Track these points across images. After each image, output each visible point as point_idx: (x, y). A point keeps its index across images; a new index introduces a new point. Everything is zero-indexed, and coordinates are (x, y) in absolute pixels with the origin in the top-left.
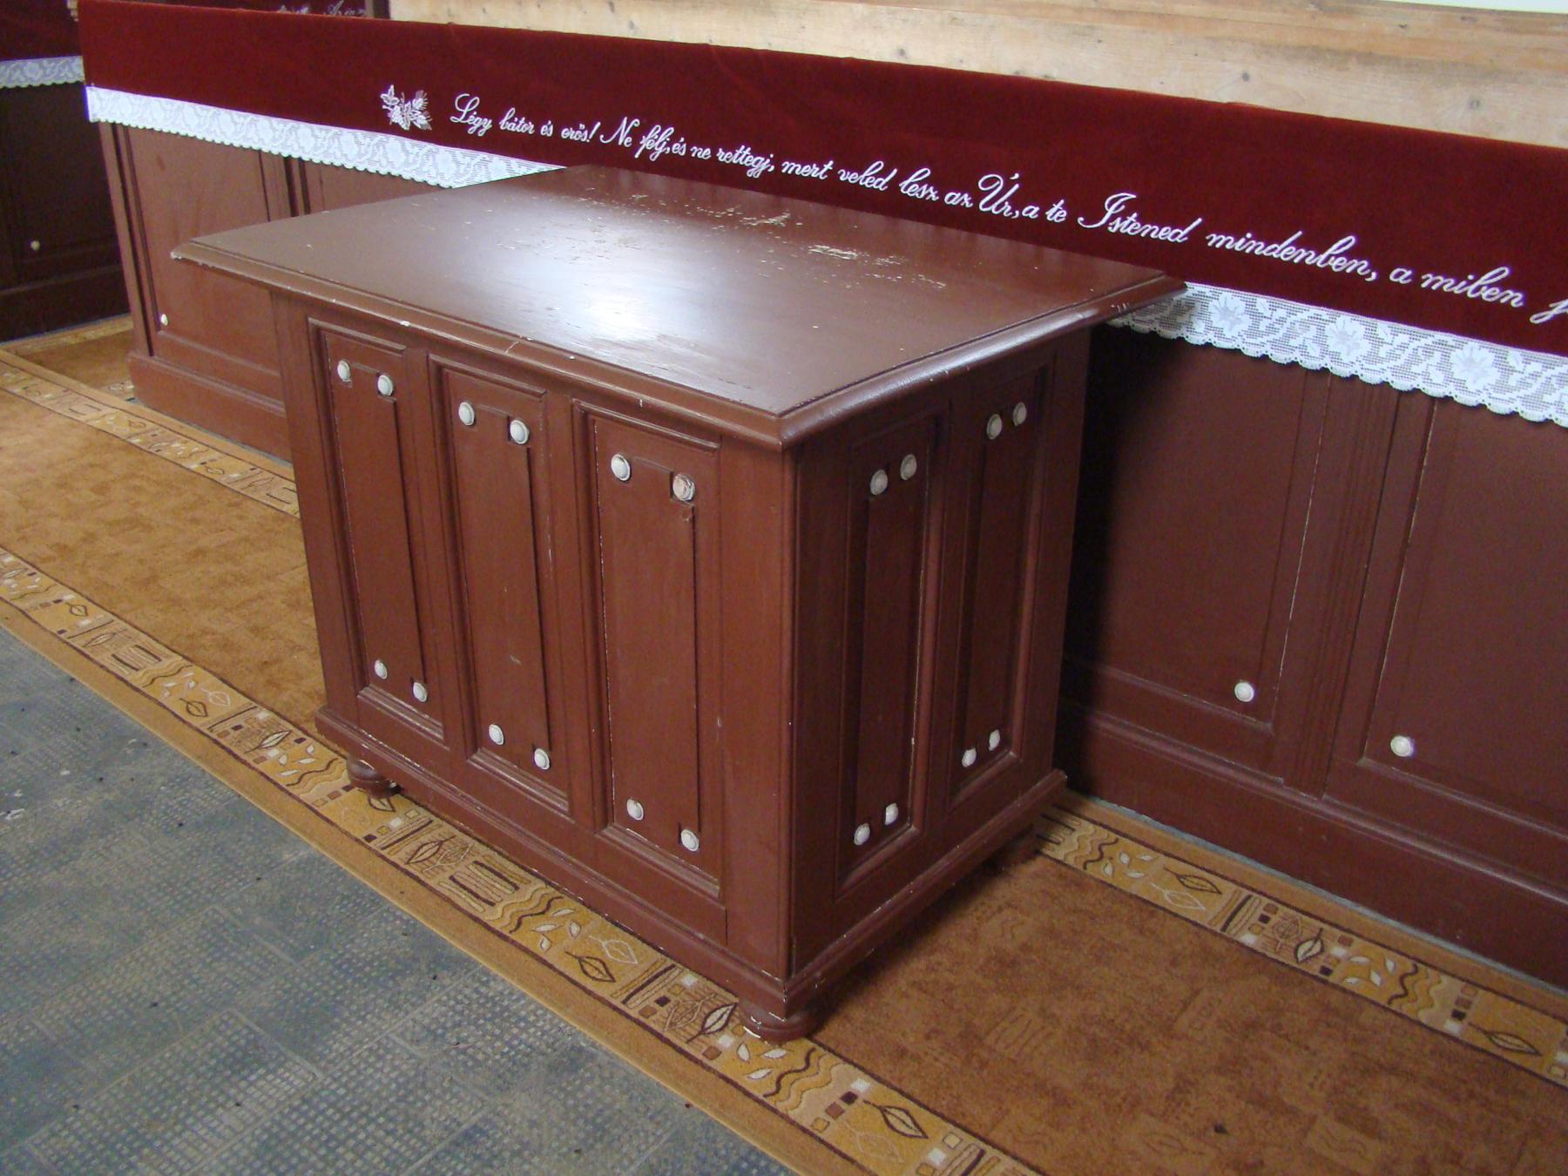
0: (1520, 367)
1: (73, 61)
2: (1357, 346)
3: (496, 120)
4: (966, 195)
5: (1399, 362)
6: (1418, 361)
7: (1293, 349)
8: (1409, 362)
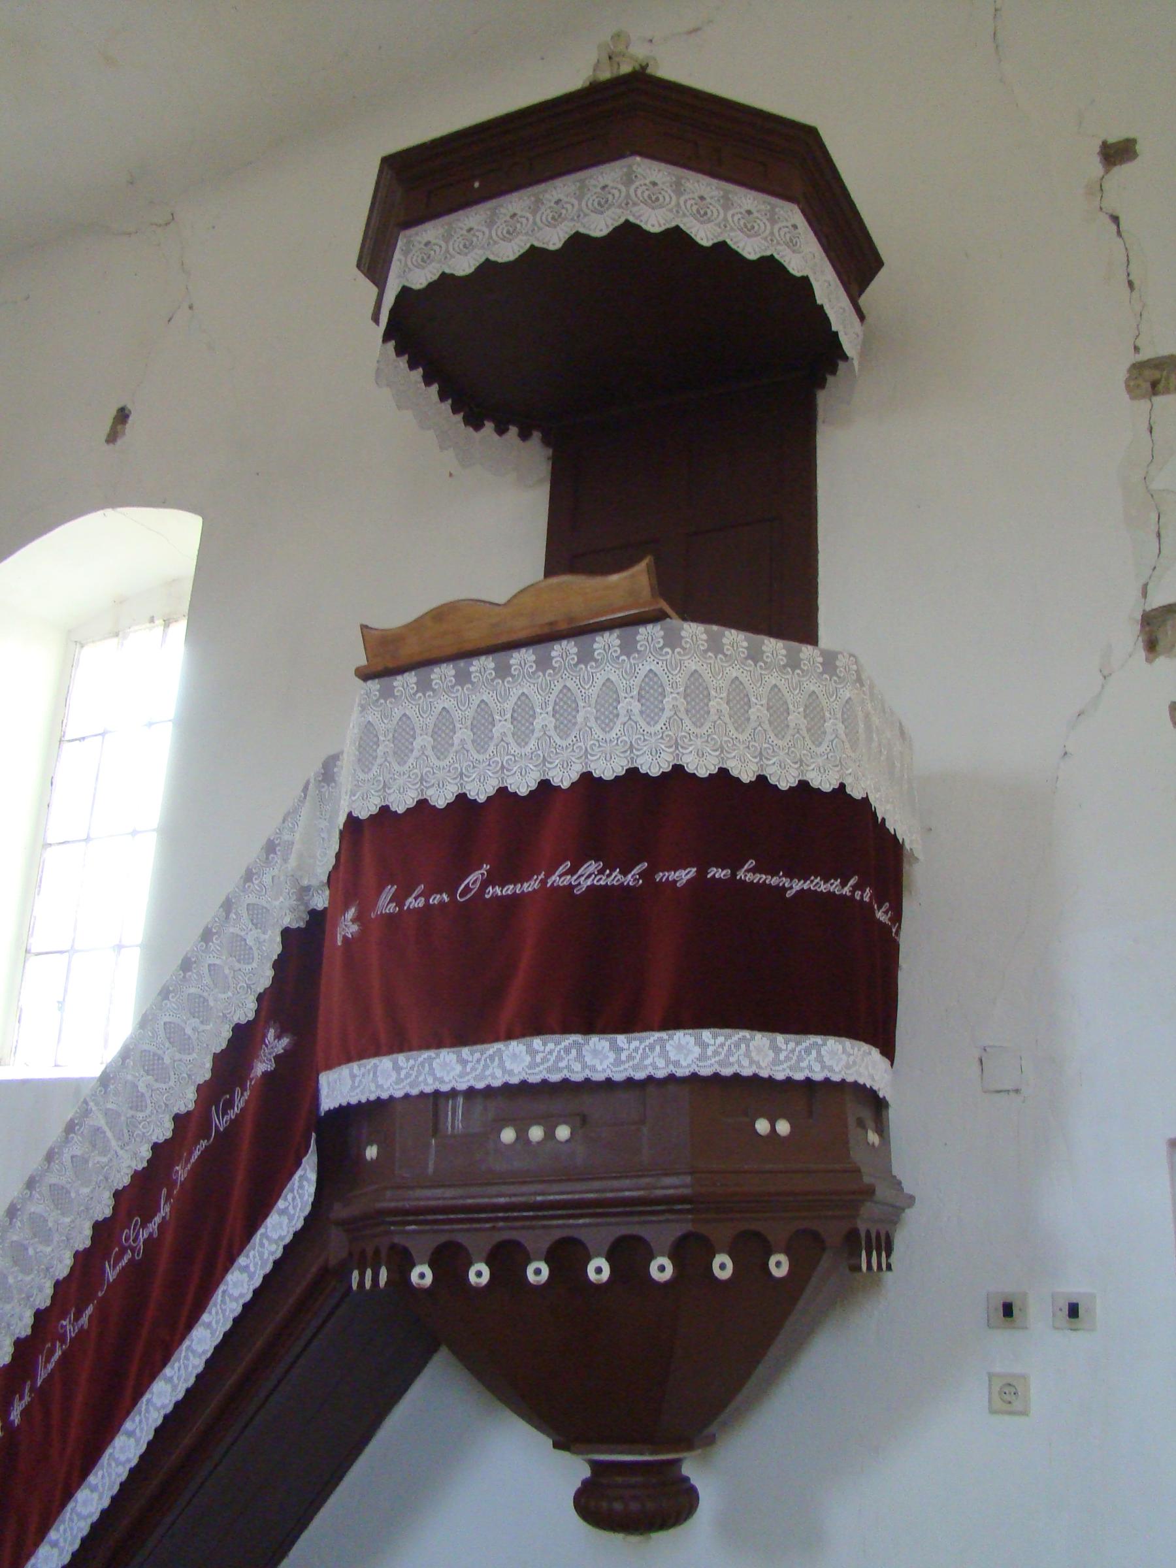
0: (712, 1042)
1: (671, 1038)
2: (690, 1051)
4: (497, 887)
5: (636, 1061)
6: (562, 1059)
7: (732, 1064)
8: (727, 1056)
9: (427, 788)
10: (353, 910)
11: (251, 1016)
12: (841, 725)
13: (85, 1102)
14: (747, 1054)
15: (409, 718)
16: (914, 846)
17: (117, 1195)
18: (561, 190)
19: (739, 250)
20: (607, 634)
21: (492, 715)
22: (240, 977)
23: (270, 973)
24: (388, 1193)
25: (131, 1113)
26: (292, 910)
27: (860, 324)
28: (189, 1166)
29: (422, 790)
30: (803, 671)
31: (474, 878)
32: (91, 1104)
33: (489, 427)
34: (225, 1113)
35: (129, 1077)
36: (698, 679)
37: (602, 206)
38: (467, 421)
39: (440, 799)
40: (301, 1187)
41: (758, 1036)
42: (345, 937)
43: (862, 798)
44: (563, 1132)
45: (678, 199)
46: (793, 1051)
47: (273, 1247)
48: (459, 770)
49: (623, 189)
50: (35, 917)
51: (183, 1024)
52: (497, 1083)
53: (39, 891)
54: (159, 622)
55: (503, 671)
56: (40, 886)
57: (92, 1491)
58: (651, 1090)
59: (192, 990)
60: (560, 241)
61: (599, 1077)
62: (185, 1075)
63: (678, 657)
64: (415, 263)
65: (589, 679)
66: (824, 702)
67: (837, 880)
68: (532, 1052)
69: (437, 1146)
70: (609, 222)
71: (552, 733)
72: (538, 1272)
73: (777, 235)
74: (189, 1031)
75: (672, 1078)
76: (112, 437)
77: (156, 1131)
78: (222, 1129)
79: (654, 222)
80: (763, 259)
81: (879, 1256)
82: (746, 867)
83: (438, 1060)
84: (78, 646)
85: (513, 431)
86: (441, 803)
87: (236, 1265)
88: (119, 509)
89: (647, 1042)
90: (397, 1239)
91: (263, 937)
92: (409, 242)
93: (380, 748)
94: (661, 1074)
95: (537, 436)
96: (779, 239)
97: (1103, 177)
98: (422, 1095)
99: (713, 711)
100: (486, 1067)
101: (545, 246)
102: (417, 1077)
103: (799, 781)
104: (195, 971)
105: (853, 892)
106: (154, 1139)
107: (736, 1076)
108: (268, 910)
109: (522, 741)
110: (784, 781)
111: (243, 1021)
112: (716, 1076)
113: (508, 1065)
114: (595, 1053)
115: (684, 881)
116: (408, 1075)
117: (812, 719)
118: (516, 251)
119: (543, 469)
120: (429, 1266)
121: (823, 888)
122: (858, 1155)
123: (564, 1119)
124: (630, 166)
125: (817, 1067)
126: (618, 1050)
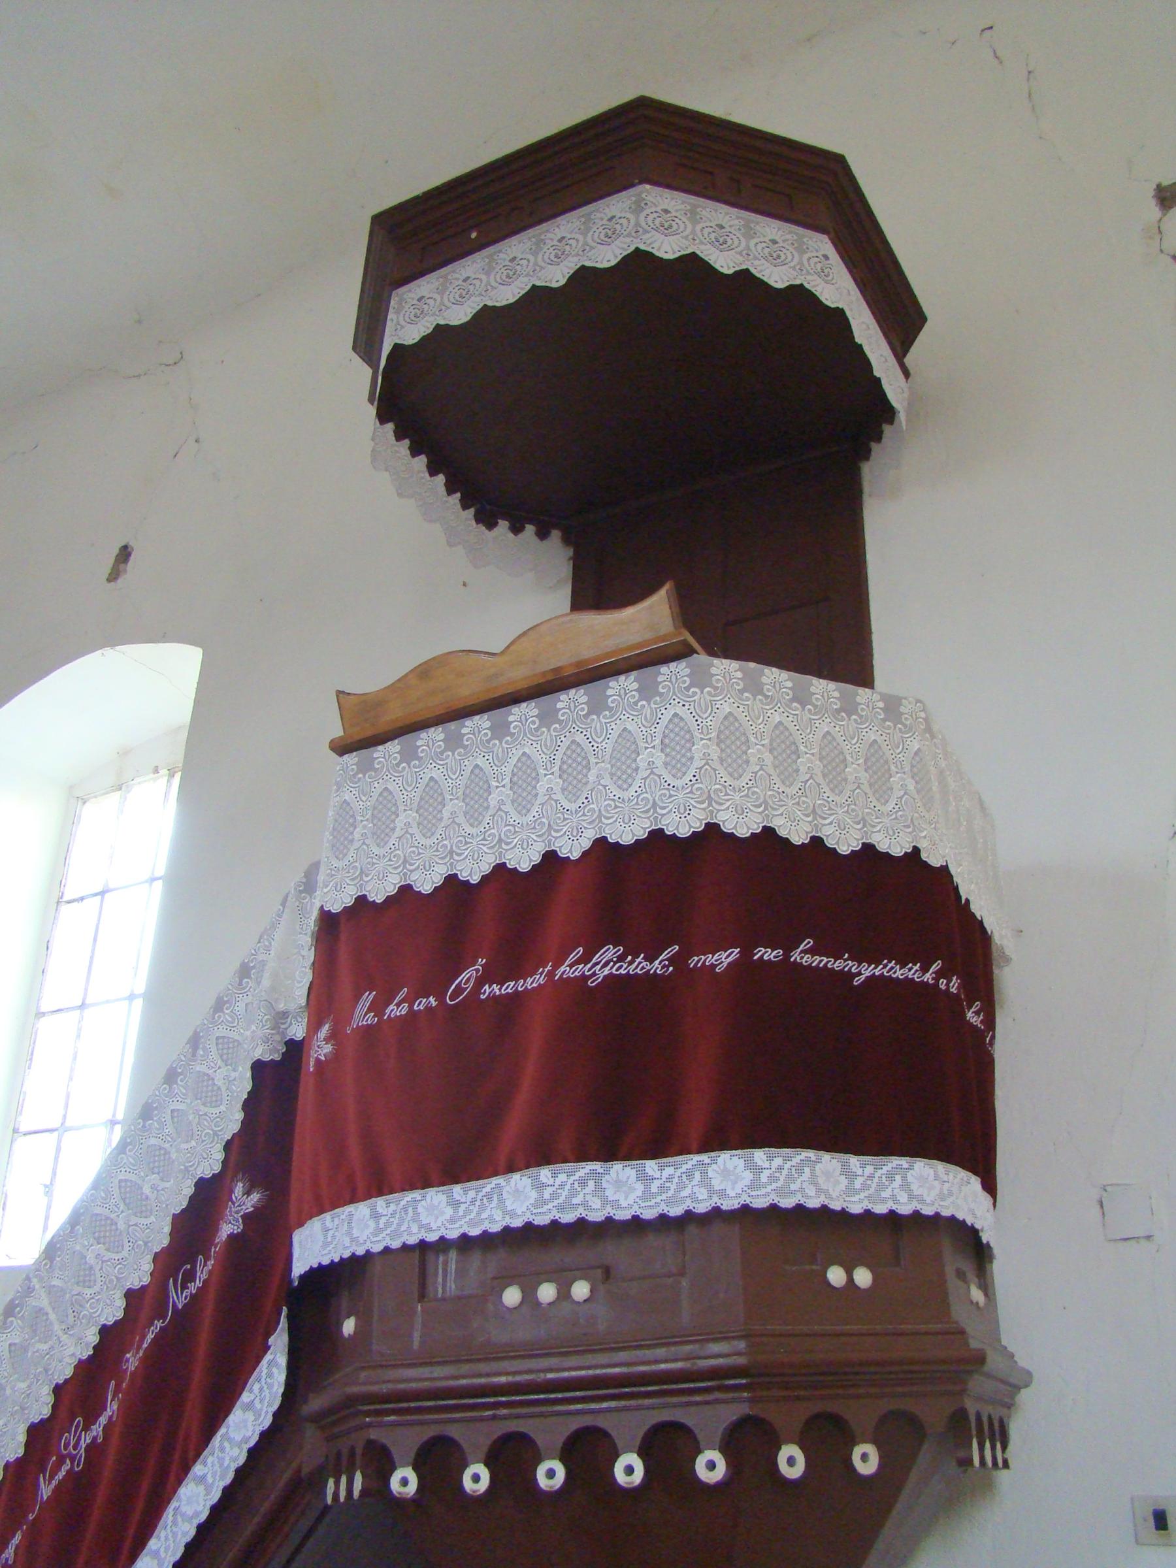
0: (767, 1165)
1: (714, 1161)
3: (788, 951)
7: (793, 1193)
9: (411, 871)
10: (327, 1026)
11: (217, 1168)
12: (910, 780)
13: (28, 1278)
14: (813, 1180)
15: (391, 793)
16: (1005, 942)
17: (58, 1390)
18: (566, 226)
19: (765, 279)
20: (622, 678)
21: (487, 782)
22: (206, 1123)
23: (239, 1116)
24: (363, 1375)
25: (77, 1289)
26: (264, 1039)
27: (905, 380)
28: (141, 1353)
29: (405, 874)
30: (861, 717)
31: (467, 977)
32: (35, 1281)
33: (503, 525)
34: (184, 1287)
35: (78, 1248)
36: (732, 724)
37: (610, 237)
38: (479, 519)
39: (426, 883)
40: (270, 1375)
41: (826, 1157)
42: (318, 1061)
43: (941, 866)
44: (581, 1290)
45: (694, 227)
46: (871, 1177)
47: (235, 1452)
48: (449, 848)
49: (632, 217)
50: (25, 1093)
51: (140, 1182)
52: (495, 1228)
53: (30, 1064)
54: (164, 772)
55: (501, 731)
56: (31, 1059)
57: (448, 1204)
58: (692, 1229)
59: (153, 1141)
60: (564, 277)
61: (623, 1215)
62: (141, 1243)
63: (708, 698)
64: (409, 321)
65: (602, 732)
66: (888, 753)
67: (916, 965)
68: (539, 1186)
69: (422, 1311)
70: (618, 252)
71: (559, 796)
72: (551, 1474)
73: (807, 265)
74: (147, 1190)
75: (716, 1212)
76: (114, 576)
77: (106, 1311)
78: (180, 1307)
79: (667, 248)
80: (791, 288)
81: (993, 1448)
82: (801, 947)
83: (423, 1203)
84: (80, 803)
85: (530, 529)
86: (426, 888)
87: (190, 1475)
88: (118, 648)
89: (684, 1167)
90: (373, 1434)
91: (234, 1075)
92: (400, 303)
93: (357, 830)
94: (702, 1208)
95: (556, 534)
96: (809, 268)
97: (1161, 220)
98: (405, 1247)
99: (753, 760)
100: (482, 1208)
101: (548, 284)
102: (399, 1225)
103: (863, 844)
104: (155, 1118)
105: (937, 979)
106: (103, 1321)
107: (800, 1208)
108: (239, 1044)
109: (524, 810)
110: (845, 843)
111: (208, 1174)
112: (774, 1207)
113: (510, 1205)
114: (618, 1183)
115: (725, 964)
116: (388, 1224)
117: (875, 773)
118: (516, 293)
119: (564, 570)
120: (413, 1469)
121: (899, 973)
122: (960, 1314)
123: (583, 1272)
124: (639, 195)
125: (903, 1197)
126: (646, 1179)
